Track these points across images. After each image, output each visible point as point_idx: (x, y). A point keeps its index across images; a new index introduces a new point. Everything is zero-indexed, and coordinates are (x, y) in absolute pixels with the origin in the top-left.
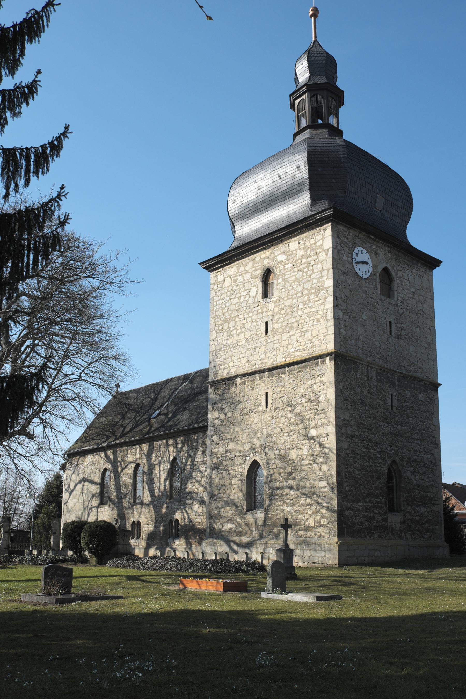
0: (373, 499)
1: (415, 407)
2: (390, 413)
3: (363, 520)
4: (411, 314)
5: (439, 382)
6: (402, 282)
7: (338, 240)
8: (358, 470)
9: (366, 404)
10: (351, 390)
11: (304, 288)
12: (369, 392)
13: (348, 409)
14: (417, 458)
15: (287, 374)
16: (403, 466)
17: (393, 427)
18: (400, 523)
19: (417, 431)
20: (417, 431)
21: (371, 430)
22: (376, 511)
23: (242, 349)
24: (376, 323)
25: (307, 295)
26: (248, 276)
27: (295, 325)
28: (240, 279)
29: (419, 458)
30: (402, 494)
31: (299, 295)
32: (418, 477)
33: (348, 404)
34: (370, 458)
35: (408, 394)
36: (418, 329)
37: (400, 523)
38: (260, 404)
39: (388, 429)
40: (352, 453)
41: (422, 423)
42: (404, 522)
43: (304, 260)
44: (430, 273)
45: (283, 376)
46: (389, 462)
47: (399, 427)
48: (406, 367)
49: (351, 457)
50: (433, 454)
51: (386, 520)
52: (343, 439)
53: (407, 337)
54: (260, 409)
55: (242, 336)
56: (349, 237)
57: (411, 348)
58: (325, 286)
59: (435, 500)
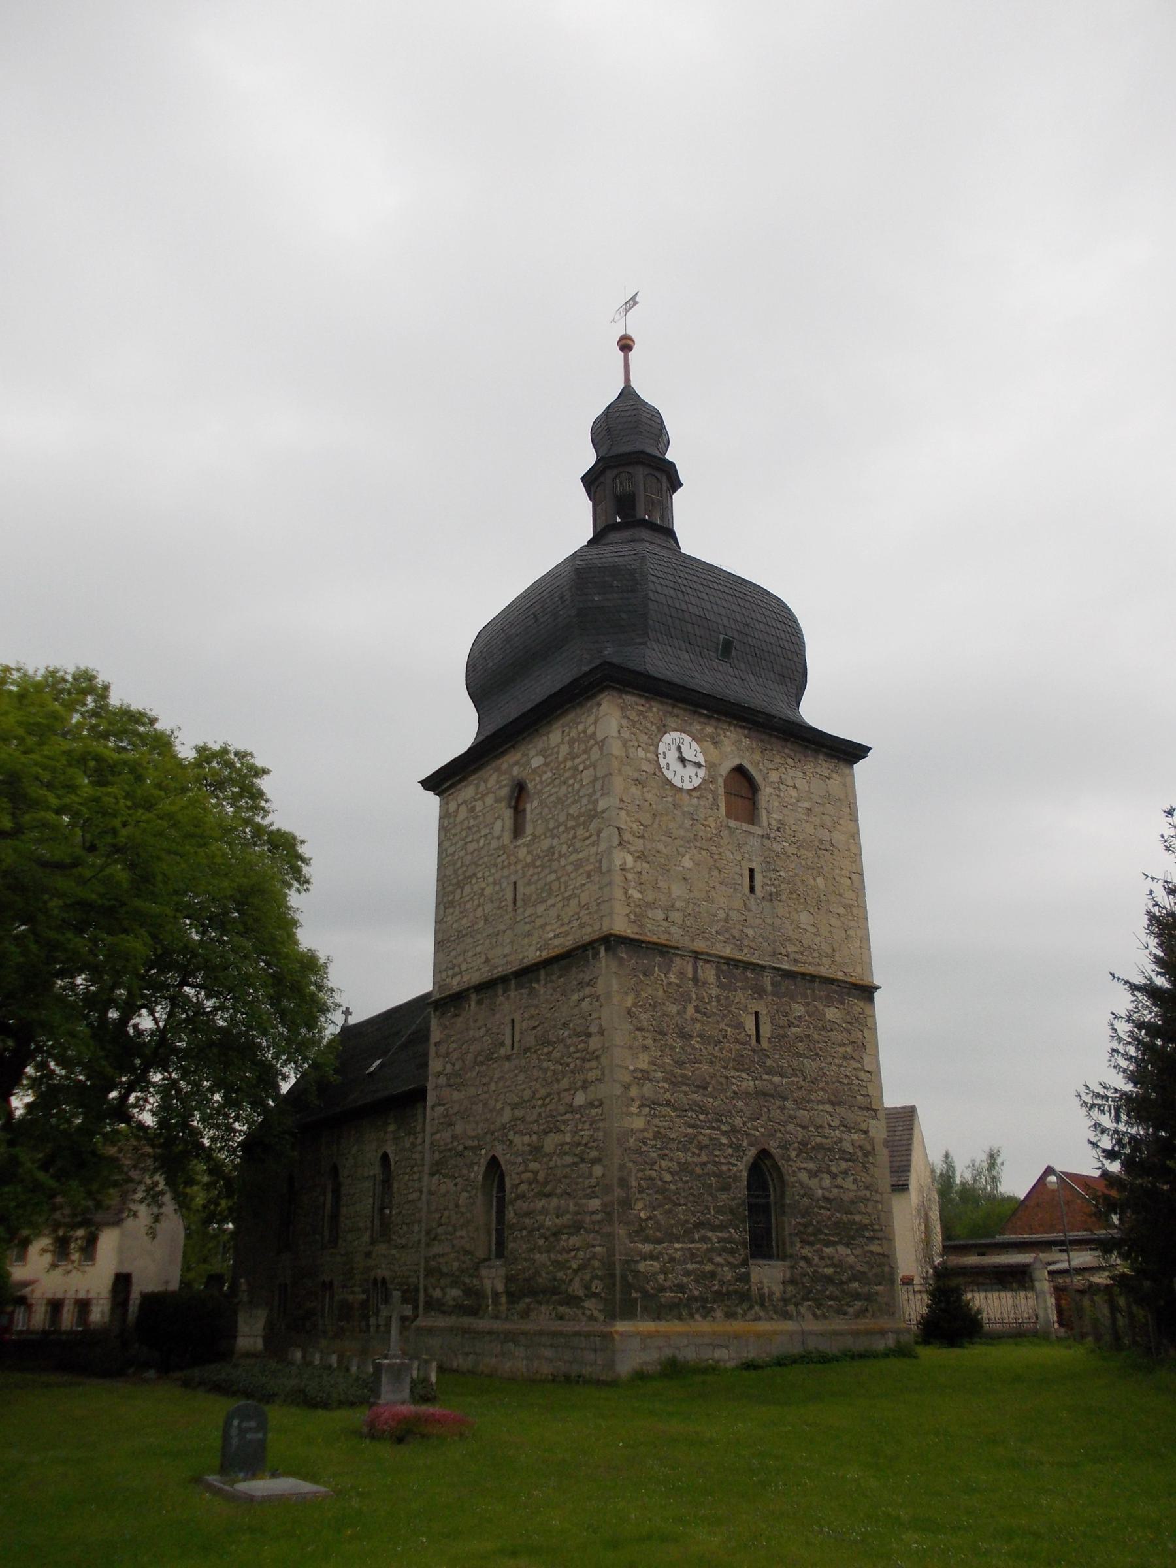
0: (710, 1234)
1: (816, 1037)
2: (754, 1051)
3: (685, 1280)
4: (803, 852)
5: (876, 982)
6: (780, 790)
7: (624, 722)
8: (671, 1172)
9: (691, 1036)
10: (655, 1007)
11: (568, 815)
12: (697, 1010)
13: (646, 1048)
14: (824, 1141)
15: (543, 982)
16: (789, 1159)
17: (762, 1080)
18: (784, 1283)
19: (822, 1085)
20: (822, 1085)
21: (706, 1088)
22: (719, 1259)
23: (479, 936)
24: (715, 873)
25: (573, 828)
26: (489, 800)
27: (555, 886)
28: (479, 806)
29: (829, 1141)
30: (785, 1219)
31: (562, 829)
32: (827, 1182)
33: (645, 1038)
34: (701, 1147)
35: (798, 1009)
36: (820, 880)
37: (784, 1283)
38: (502, 1044)
39: (749, 1084)
40: (655, 1138)
41: (834, 1068)
42: (792, 1282)
43: (569, 764)
44: (847, 771)
45: (536, 985)
46: (752, 1152)
47: (776, 1079)
48: (792, 956)
49: (654, 1146)
50: (866, 1132)
51: (745, 1278)
52: (634, 1109)
53: (794, 896)
54: (502, 1051)
55: (479, 913)
56: (650, 715)
57: (804, 918)
58: (599, 809)
59: (873, 1230)
